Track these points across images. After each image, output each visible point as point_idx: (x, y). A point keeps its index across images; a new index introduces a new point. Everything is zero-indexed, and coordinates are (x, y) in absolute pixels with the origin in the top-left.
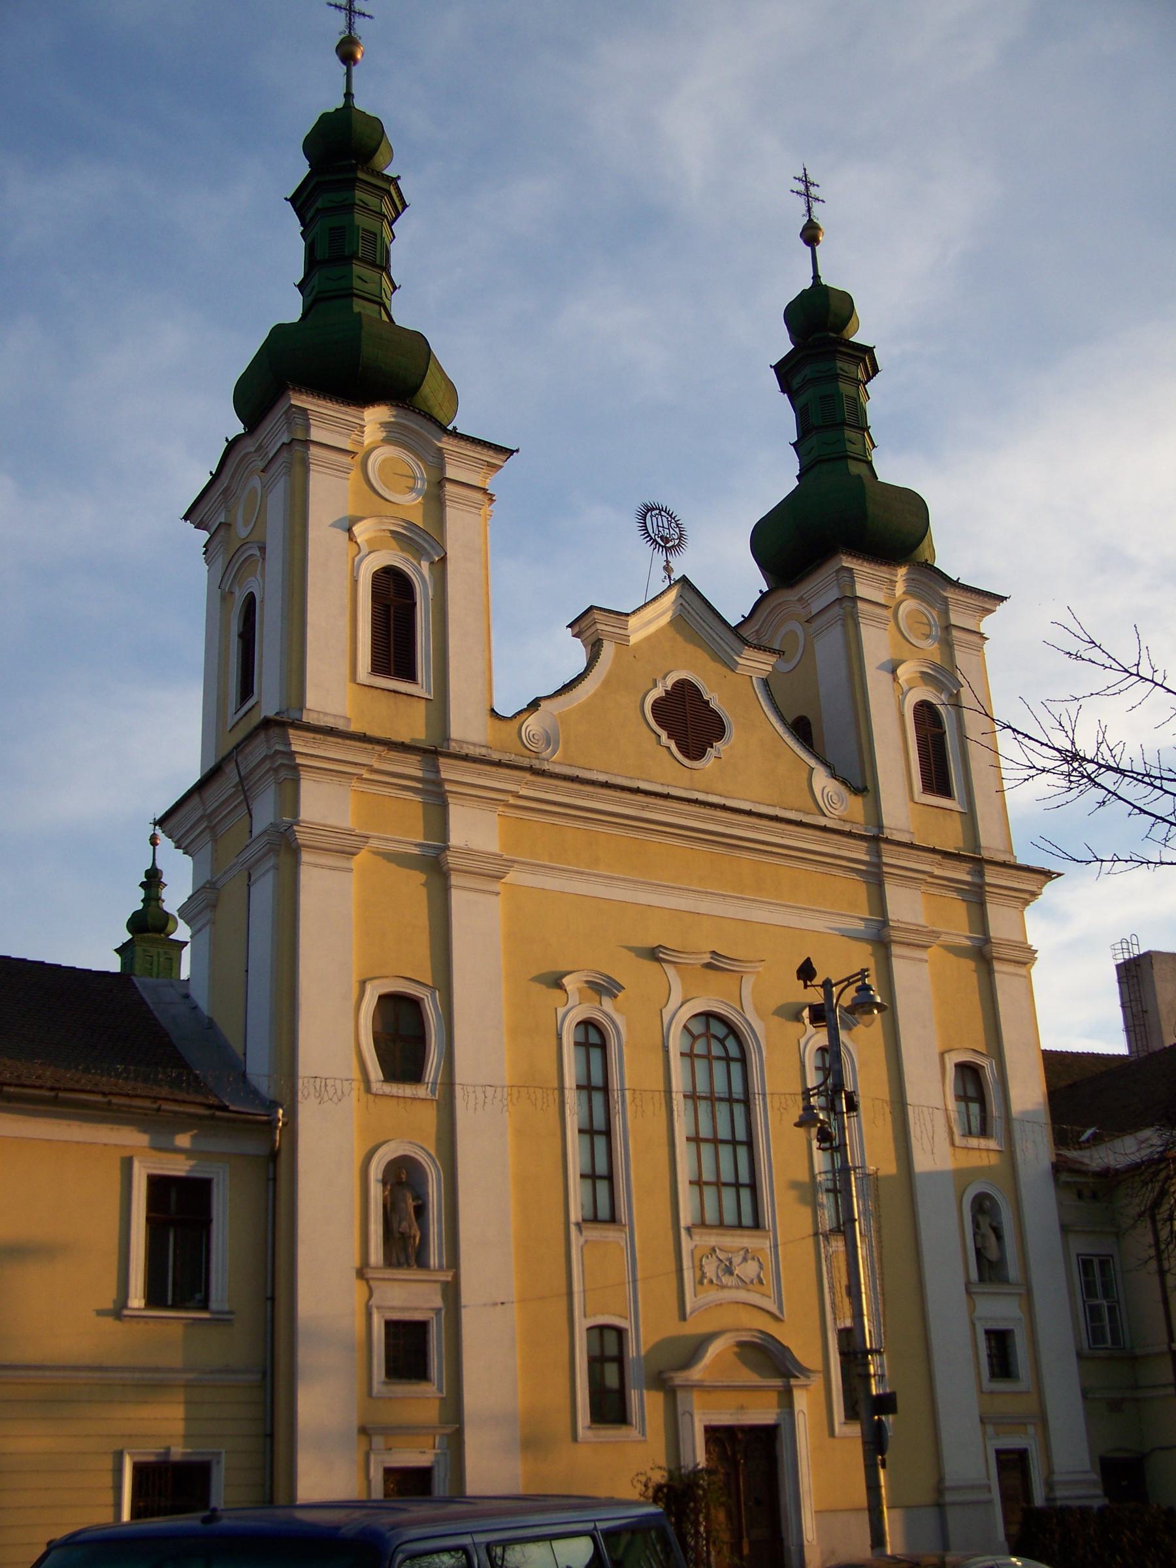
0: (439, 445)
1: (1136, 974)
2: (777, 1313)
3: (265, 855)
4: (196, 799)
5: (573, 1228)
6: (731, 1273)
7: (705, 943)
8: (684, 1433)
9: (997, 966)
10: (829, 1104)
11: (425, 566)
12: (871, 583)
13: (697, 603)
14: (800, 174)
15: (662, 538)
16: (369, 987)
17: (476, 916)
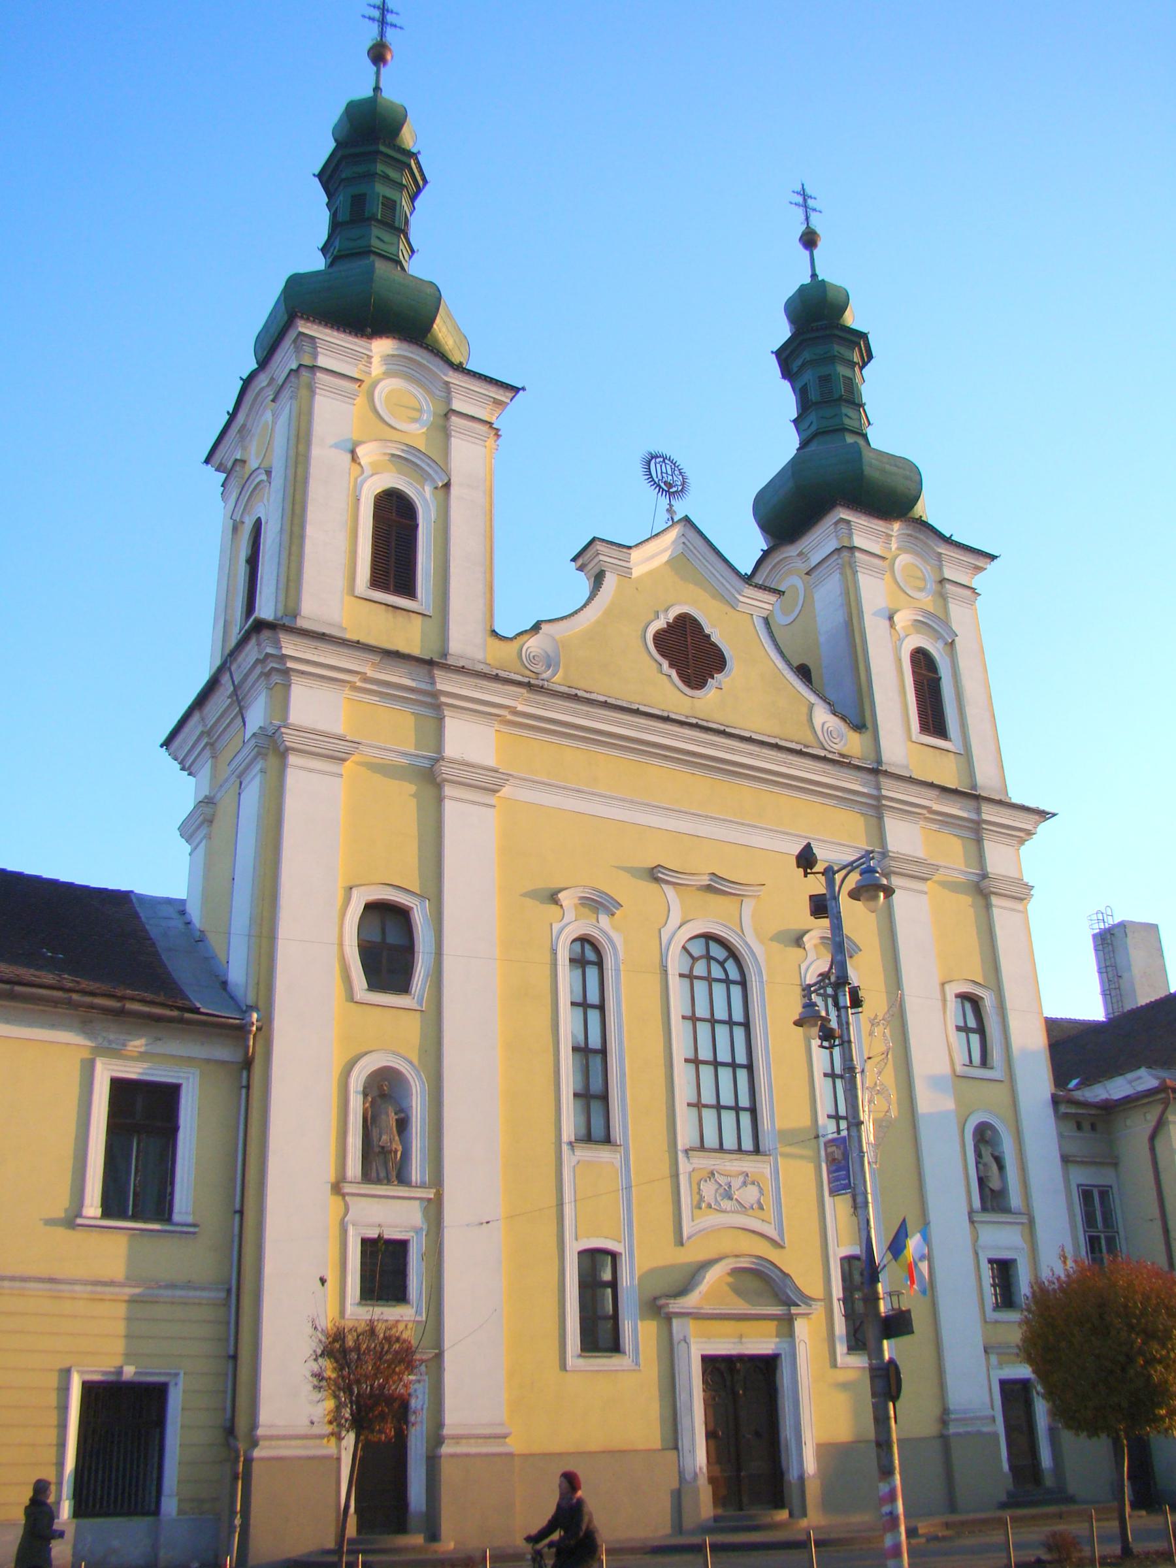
0: (446, 379)
1: (1110, 943)
2: (777, 1238)
4: (196, 717)
5: (565, 1148)
6: (730, 1198)
7: (702, 866)
9: (994, 900)
10: (830, 1005)
11: (428, 489)
12: (867, 533)
13: (699, 542)
14: (799, 188)
15: (665, 483)
16: (355, 892)
17: (468, 824)
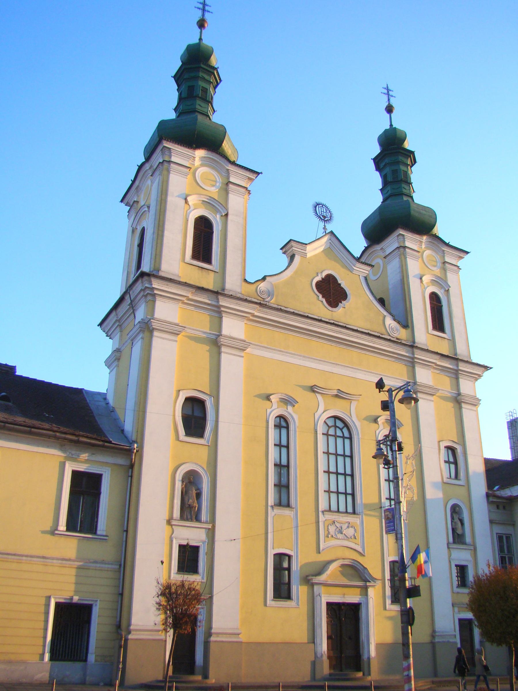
2: (362, 552)
3: (139, 333)
4: (114, 313)
5: (269, 508)
6: (342, 533)
7: (334, 386)
8: (317, 606)
10: (389, 449)
12: (411, 240)
14: (385, 86)
15: (323, 216)
16: (181, 393)
17: (232, 365)
